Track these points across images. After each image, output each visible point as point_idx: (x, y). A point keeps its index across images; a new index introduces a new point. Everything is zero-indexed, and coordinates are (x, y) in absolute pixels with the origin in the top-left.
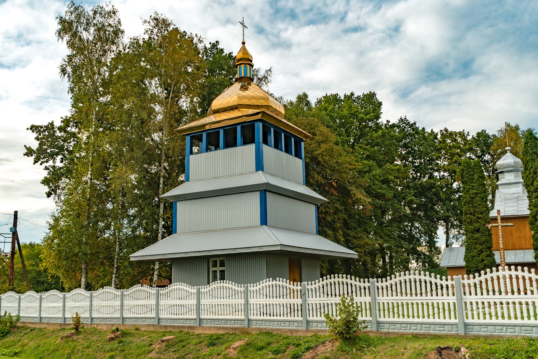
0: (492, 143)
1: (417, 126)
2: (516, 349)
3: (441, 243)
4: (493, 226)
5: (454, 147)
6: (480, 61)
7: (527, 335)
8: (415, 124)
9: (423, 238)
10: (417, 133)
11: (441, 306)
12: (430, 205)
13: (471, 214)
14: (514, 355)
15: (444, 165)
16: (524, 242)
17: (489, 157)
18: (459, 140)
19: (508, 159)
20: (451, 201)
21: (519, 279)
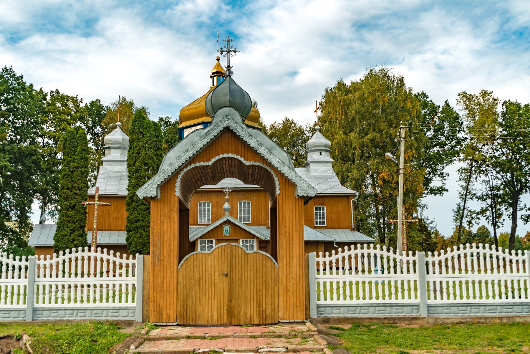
0: (104, 115)
1: (24, 80)
2: (82, 334)
3: (34, 218)
4: (89, 204)
5: (64, 112)
6: (104, 23)
7: (97, 318)
8: (22, 77)
9: (13, 212)
10: (23, 89)
11: (9, 290)
12: (27, 174)
13: (68, 189)
14: (78, 340)
15: (50, 131)
16: (120, 223)
17: (100, 129)
18: (71, 105)
19: (117, 135)
20: (53, 172)
21: (103, 261)
